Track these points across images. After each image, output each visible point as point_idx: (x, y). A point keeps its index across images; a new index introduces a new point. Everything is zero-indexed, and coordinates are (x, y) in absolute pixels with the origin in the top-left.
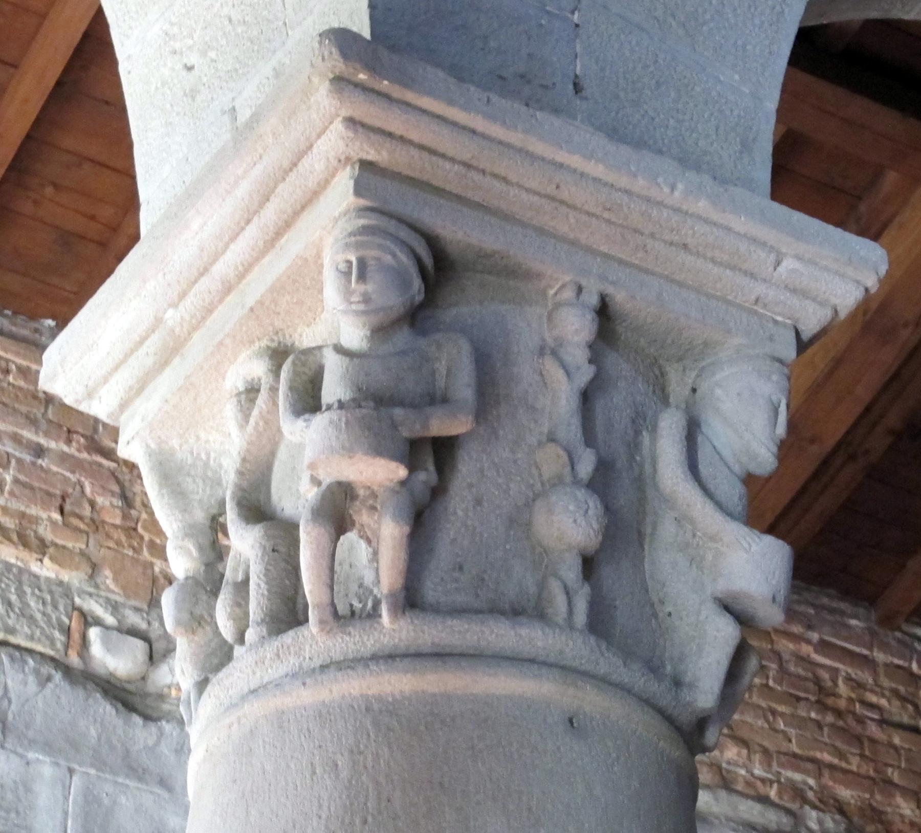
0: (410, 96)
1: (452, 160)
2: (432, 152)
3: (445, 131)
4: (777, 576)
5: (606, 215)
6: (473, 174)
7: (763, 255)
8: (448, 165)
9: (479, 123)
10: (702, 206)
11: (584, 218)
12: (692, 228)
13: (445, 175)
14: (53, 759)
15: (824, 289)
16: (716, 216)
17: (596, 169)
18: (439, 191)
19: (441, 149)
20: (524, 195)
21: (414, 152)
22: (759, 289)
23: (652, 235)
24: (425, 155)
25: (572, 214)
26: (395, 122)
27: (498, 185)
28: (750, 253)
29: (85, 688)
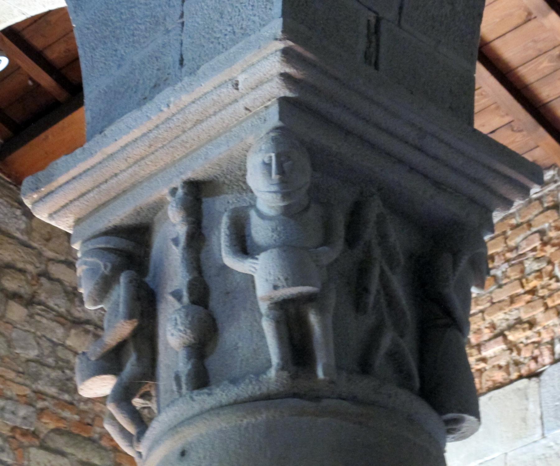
0: (55, 184)
1: (89, 191)
2: (83, 195)
3: (75, 183)
4: (20, 250)
5: (153, 148)
6: (103, 187)
7: (224, 90)
8: (91, 195)
9: (74, 172)
10: (186, 98)
11: (152, 157)
12: (190, 113)
13: (94, 199)
14: (138, 396)
15: (261, 74)
16: (194, 96)
17: (136, 133)
18: (104, 205)
19: (84, 190)
20: (125, 174)
21: (77, 203)
22: (241, 104)
23: (184, 132)
24: (81, 200)
25: (147, 161)
26: (70, 193)
27: (114, 181)
28: (219, 96)
29: (29, 295)
